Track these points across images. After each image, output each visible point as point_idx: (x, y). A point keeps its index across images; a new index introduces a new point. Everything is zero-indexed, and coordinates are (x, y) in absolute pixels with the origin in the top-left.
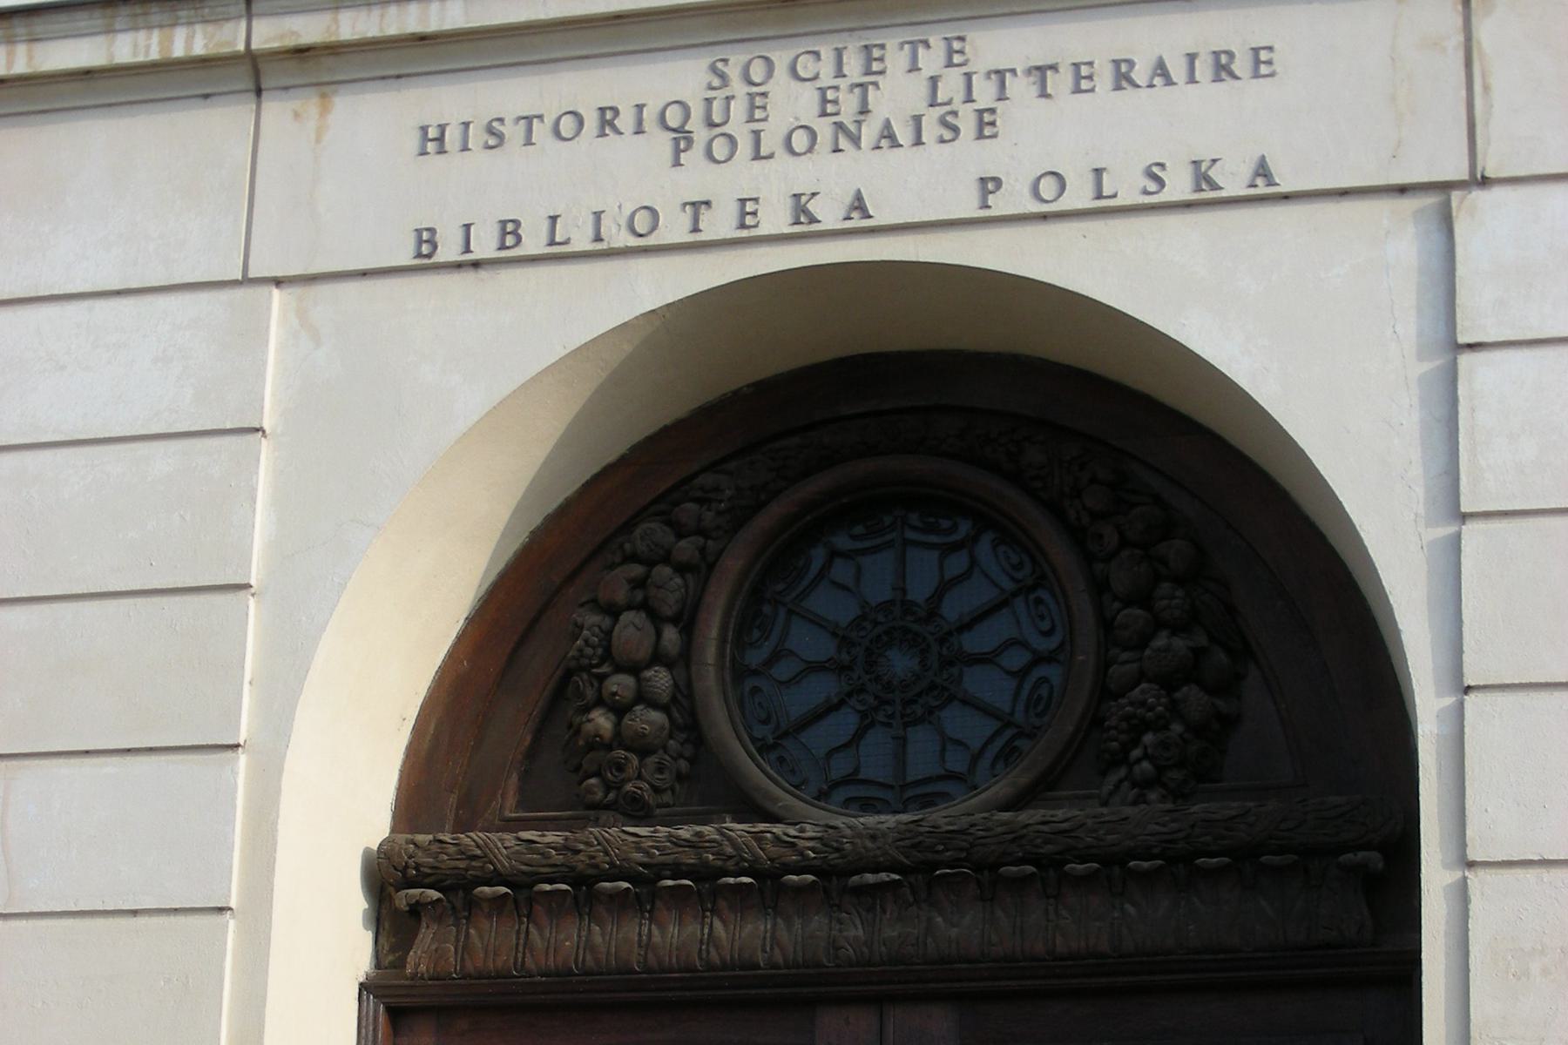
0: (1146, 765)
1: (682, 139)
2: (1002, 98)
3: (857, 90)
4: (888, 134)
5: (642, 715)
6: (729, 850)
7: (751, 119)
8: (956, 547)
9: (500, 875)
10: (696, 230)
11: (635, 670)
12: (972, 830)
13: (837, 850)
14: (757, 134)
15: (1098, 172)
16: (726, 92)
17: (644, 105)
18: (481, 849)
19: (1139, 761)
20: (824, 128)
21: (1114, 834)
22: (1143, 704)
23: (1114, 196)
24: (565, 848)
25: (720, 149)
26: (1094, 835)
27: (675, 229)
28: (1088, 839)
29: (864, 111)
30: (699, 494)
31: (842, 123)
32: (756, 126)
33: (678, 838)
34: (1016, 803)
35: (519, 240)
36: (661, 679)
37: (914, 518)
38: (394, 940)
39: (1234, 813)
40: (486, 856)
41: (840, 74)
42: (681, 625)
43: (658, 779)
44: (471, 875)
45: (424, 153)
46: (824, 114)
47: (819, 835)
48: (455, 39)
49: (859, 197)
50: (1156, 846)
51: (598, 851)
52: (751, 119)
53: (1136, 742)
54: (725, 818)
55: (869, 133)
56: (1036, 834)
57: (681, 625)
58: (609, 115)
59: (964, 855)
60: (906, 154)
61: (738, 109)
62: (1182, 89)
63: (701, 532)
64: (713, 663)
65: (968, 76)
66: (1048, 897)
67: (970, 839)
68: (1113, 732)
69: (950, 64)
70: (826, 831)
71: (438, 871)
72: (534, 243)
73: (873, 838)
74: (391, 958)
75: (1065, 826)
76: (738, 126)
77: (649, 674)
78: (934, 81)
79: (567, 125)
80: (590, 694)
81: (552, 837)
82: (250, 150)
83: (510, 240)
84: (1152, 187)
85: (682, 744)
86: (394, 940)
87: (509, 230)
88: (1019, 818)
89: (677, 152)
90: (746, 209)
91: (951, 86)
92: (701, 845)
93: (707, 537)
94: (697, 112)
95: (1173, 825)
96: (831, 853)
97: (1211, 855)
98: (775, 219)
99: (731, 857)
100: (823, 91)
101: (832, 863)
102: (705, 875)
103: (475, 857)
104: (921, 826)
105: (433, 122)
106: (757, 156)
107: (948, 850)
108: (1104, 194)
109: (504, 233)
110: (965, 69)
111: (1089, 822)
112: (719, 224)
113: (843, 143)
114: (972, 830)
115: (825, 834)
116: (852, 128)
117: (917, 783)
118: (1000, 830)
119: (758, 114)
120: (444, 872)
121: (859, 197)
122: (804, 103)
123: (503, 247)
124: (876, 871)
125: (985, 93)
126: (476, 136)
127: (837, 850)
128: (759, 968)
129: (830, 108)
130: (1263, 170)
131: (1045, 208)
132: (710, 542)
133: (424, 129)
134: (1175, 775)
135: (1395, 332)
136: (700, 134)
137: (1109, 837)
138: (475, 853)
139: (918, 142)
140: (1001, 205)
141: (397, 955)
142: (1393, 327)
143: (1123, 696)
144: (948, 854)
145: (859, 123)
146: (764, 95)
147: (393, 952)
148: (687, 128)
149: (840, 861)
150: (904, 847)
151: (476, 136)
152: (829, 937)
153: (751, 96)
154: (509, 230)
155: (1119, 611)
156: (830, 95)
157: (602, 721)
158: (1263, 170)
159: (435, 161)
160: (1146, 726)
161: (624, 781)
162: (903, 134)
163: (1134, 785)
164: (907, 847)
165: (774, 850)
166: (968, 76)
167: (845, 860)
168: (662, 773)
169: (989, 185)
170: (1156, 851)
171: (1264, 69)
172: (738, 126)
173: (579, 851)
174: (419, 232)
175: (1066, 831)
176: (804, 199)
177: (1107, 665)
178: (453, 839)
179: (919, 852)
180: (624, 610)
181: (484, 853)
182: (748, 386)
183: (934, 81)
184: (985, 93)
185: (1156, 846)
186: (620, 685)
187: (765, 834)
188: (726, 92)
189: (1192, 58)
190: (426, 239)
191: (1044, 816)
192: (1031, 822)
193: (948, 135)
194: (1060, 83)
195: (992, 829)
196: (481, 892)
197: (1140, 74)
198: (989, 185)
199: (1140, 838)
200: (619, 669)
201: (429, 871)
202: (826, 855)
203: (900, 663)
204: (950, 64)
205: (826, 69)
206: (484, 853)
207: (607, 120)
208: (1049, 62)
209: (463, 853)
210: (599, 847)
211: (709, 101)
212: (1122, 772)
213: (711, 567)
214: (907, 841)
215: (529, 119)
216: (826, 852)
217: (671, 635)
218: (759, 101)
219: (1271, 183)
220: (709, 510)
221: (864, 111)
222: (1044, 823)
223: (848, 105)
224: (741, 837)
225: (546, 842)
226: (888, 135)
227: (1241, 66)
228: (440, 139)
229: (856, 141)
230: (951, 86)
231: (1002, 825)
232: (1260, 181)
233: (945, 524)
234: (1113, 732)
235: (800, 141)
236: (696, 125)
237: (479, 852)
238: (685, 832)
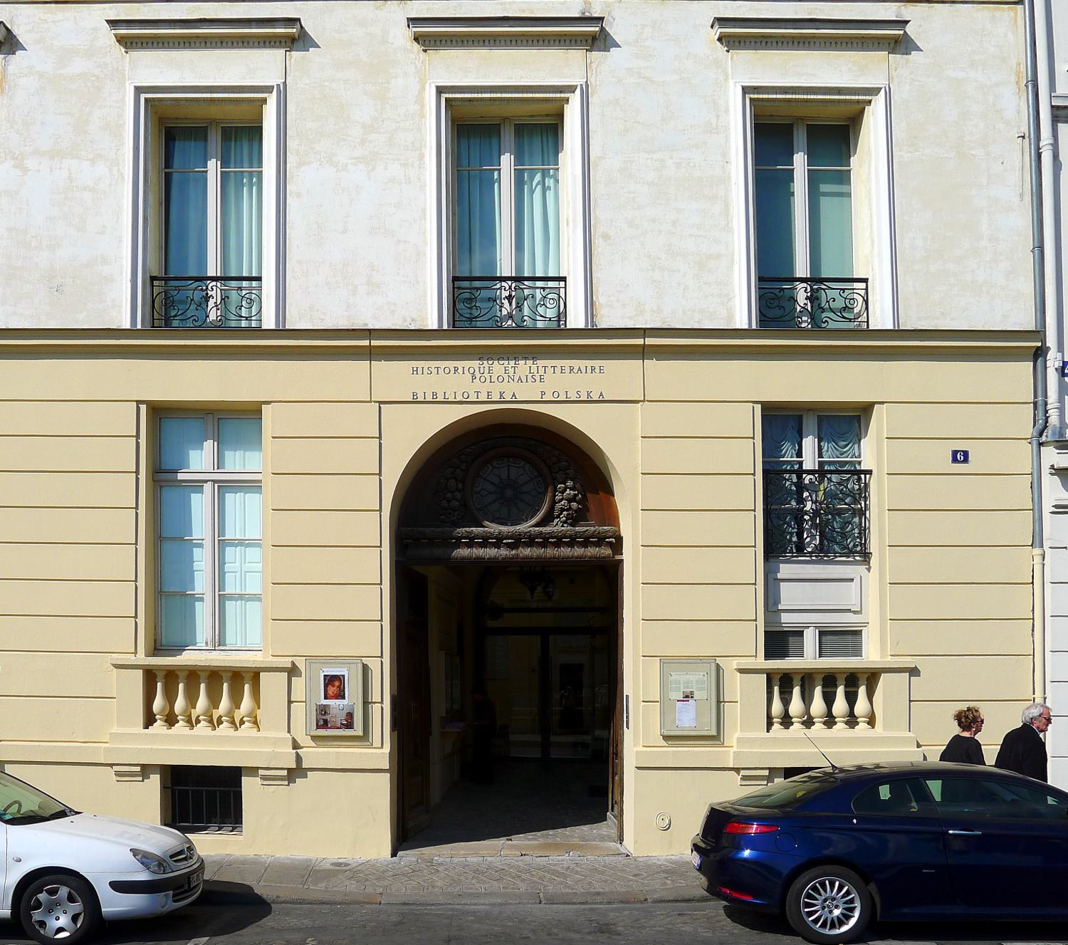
1: (474, 377)
2: (545, 373)
4: (520, 379)
7: (489, 373)
14: (491, 376)
34: (537, 525)
36: (458, 495)
37: (511, 460)
45: (413, 374)
52: (489, 373)
53: (562, 514)
77: (454, 493)
82: (992, 5)
94: (477, 370)
102: (472, 539)
119: (491, 372)
131: (464, 400)
133: (413, 368)
136: (478, 375)
139: (527, 382)
157: (445, 503)
160: (564, 510)
162: (524, 380)
169: (543, 393)
171: (542, 380)
186: (449, 495)
198: (543, 393)
203: (509, 493)
217: (460, 485)
226: (520, 379)
228: (417, 371)
236: (477, 373)
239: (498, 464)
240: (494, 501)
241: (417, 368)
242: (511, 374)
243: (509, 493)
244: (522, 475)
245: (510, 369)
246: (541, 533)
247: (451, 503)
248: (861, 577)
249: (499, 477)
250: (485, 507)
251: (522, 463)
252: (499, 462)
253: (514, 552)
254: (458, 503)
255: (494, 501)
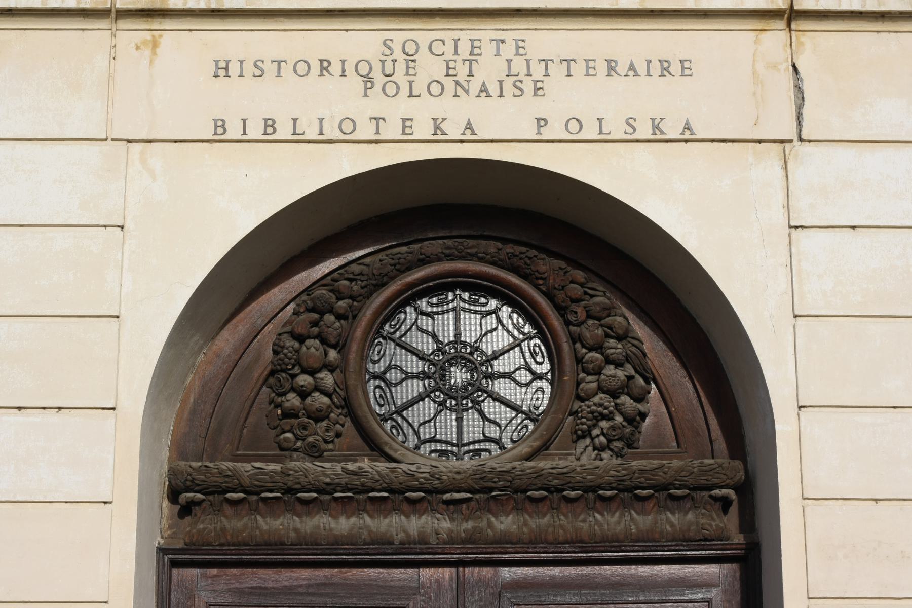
0: (602, 438)
1: (368, 80)
2: (547, 75)
3: (543, 63)
4: (484, 90)
5: (319, 399)
6: (377, 477)
7: (407, 74)
8: (489, 313)
9: (242, 486)
10: (377, 133)
11: (312, 373)
12: (513, 471)
13: (439, 479)
14: (411, 83)
15: (295, 120)
16: (391, 57)
17: (345, 61)
18: (231, 472)
19: (598, 436)
20: (449, 83)
21: (592, 476)
22: (601, 405)
23: (303, 134)
24: (284, 473)
25: (390, 89)
26: (581, 476)
27: (366, 131)
28: (578, 478)
29: (471, 74)
30: (351, 276)
31: (458, 81)
32: (411, 78)
33: (346, 469)
35: (275, 131)
36: (327, 379)
37: (466, 296)
38: (171, 522)
39: (655, 466)
40: (234, 476)
41: (456, 53)
42: (338, 349)
43: (327, 436)
44: (224, 486)
46: (448, 75)
47: (428, 471)
48: (464, 13)
49: (469, 123)
50: (614, 483)
51: (302, 475)
53: (595, 426)
54: (364, 459)
55: (475, 87)
56: (549, 474)
57: (338, 349)
58: (325, 64)
59: (509, 484)
60: (494, 101)
61: (401, 68)
62: (643, 78)
63: (352, 298)
64: (299, 371)
65: (528, 61)
66: (553, 509)
67: (512, 475)
68: (584, 420)
69: (517, 54)
70: (432, 469)
71: (205, 483)
72: (284, 132)
73: (458, 473)
74: (169, 532)
75: (565, 470)
76: (400, 76)
78: (509, 62)
79: (302, 68)
80: (287, 386)
81: (273, 467)
83: (270, 130)
84: (630, 130)
85: (338, 416)
86: (171, 522)
87: (269, 124)
88: (539, 465)
89: (366, 89)
90: (406, 123)
91: (519, 66)
92: (360, 474)
93: (354, 300)
94: (377, 67)
95: (623, 472)
96: (434, 481)
97: (644, 489)
98: (423, 130)
99: (377, 481)
100: (447, 62)
101: (435, 486)
103: (228, 476)
104: (485, 467)
105: (222, 57)
106: (411, 95)
107: (500, 481)
108: (603, 132)
109: (266, 126)
110: (525, 57)
111: (578, 469)
112: (392, 131)
113: (460, 91)
114: (513, 471)
115: (431, 470)
116: (465, 84)
117: (469, 444)
118: (529, 471)
120: (209, 484)
121: (469, 123)
122: (437, 69)
123: (265, 133)
124: (458, 492)
125: (538, 71)
126: (249, 68)
127: (439, 479)
128: (393, 544)
129: (451, 72)
130: (688, 127)
132: (355, 303)
133: (217, 62)
134: (618, 444)
135: (757, 217)
136: (379, 79)
137: (589, 477)
138: (227, 474)
140: (547, 134)
141: (173, 531)
142: (756, 214)
143: (588, 400)
144: (501, 483)
145: (468, 81)
146: (413, 61)
147: (170, 529)
148: (370, 76)
149: (439, 485)
150: (475, 479)
151: (249, 68)
152: (432, 527)
153: (407, 61)
154: (269, 124)
155: (586, 353)
156: (451, 65)
157: (293, 400)
158: (688, 127)
159: (222, 80)
160: (604, 417)
161: (307, 436)
162: (493, 89)
163: (595, 449)
164: (477, 479)
165: (402, 478)
166: (528, 61)
167: (442, 485)
168: (328, 432)
169: (542, 122)
170: (614, 485)
172: (400, 76)
173: (289, 475)
174: (266, 120)
175: (566, 473)
176: (438, 122)
177: (578, 384)
178: (214, 465)
179: (484, 482)
180: (307, 339)
181: (233, 474)
182: (375, 217)
183: (509, 62)
184: (538, 71)
185: (614, 483)
186: (304, 380)
187: (396, 469)
188: (391, 57)
189: (649, 62)
190: (220, 125)
191: (552, 465)
192: (545, 467)
193: (518, 92)
194: (578, 69)
195: (525, 471)
196: (231, 496)
197: (622, 68)
198: (542, 122)
199: (607, 478)
200: (304, 371)
201: (200, 483)
202: (432, 482)
203: (458, 376)
204: (517, 54)
205: (449, 48)
206: (233, 474)
207: (325, 67)
208: (283, 59)
209: (221, 473)
210: (301, 473)
211: (383, 62)
212: (588, 441)
213: (354, 317)
214: (477, 476)
215: (279, 62)
216: (431, 480)
218: (411, 64)
219: (473, 133)
220: (356, 284)
221: (471, 74)
222: (553, 468)
223: (462, 72)
224: (383, 470)
225: (270, 469)
226: (484, 90)
227: (675, 68)
228: (226, 69)
229: (467, 92)
230: (519, 66)
231: (530, 469)
232: (468, 132)
233: (483, 300)
234: (584, 420)
235: (436, 89)
237: (230, 473)
238: (351, 466)
239: (432, 305)
240: (420, 398)
241: (228, 62)
242: (462, 78)
243: (458, 376)
244: (492, 331)
245: (459, 64)
246: (539, 473)
247: (309, 400)
248: (112, 511)
249: (434, 336)
250: (399, 412)
251: (493, 303)
252: (435, 300)
253: (469, 525)
254: (326, 400)
255: (420, 398)
